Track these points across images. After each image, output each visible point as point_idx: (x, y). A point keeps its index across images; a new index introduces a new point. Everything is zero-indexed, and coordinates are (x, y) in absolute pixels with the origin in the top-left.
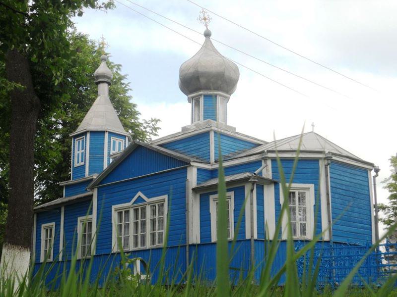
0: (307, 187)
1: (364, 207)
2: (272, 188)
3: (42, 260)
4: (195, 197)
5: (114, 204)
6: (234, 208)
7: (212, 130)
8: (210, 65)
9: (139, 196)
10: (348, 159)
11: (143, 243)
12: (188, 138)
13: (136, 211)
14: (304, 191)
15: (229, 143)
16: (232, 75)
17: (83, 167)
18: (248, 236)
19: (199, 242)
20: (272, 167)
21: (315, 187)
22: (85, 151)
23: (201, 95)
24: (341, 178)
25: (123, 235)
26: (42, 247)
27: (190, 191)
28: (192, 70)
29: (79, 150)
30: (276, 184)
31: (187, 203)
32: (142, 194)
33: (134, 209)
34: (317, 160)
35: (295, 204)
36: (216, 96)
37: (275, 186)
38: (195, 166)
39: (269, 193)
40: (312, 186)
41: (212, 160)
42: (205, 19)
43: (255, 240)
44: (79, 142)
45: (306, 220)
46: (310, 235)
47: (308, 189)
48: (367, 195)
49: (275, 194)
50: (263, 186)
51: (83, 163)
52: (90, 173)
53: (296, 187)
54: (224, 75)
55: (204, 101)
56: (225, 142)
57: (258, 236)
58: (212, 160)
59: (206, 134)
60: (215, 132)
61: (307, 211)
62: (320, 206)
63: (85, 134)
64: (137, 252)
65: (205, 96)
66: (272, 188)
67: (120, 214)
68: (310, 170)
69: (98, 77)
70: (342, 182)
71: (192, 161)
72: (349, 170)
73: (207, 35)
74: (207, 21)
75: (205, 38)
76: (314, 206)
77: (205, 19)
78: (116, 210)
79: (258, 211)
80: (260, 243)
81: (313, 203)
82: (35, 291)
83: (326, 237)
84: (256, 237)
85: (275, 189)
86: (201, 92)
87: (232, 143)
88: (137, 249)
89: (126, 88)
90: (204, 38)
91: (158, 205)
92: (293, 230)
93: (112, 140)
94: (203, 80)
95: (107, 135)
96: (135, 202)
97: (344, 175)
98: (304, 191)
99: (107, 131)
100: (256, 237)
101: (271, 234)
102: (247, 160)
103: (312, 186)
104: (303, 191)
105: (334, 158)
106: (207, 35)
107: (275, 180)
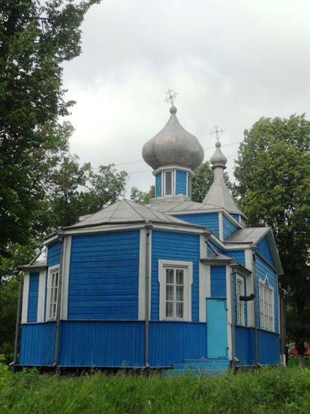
6: (192, 283)
11: (180, 312)
14: (172, 268)
18: (141, 317)
24: (91, 249)
25: (175, 298)
26: (40, 288)
32: (162, 260)
34: (138, 231)
38: (69, 235)
47: (186, 267)
60: (224, 215)
64: (181, 325)
67: (169, 273)
72: (128, 237)
73: (173, 111)
80: (32, 327)
81: (191, 282)
82: (192, 359)
84: (149, 319)
88: (169, 319)
91: (177, 271)
100: (149, 319)
105: (155, 226)
106: (173, 111)
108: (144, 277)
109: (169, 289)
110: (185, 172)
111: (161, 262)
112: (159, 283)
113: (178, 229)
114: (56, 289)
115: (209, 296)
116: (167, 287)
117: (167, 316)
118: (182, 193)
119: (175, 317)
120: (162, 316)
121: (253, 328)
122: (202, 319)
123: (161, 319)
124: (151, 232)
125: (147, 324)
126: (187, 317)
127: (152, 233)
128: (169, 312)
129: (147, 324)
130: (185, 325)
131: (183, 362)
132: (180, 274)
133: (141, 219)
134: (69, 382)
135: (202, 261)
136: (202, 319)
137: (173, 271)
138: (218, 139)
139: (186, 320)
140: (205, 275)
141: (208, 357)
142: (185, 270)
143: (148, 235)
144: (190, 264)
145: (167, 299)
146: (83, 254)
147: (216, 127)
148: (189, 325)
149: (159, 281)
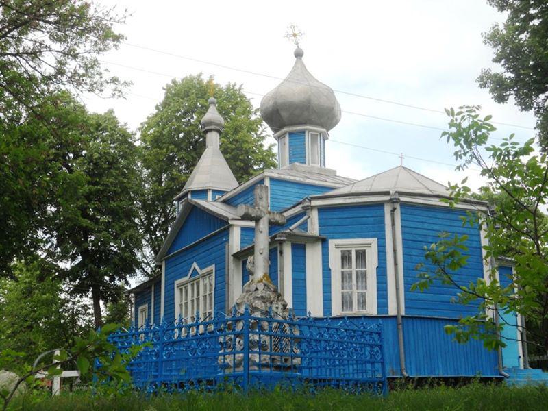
0: (367, 242)
1: (469, 265)
2: (319, 247)
4: (237, 266)
5: (176, 280)
7: (266, 176)
8: (296, 93)
10: (437, 199)
11: (363, 302)
12: (249, 188)
14: (365, 248)
15: (296, 191)
16: (324, 102)
20: (319, 219)
21: (378, 242)
24: (426, 226)
27: (231, 258)
28: (271, 103)
30: (324, 241)
31: (227, 273)
34: (380, 205)
35: (351, 268)
36: (303, 132)
37: (322, 244)
38: (238, 226)
39: (313, 256)
40: (374, 241)
42: (295, 35)
43: (403, 317)
45: (366, 289)
47: (369, 245)
48: (476, 248)
49: (323, 255)
50: (305, 245)
53: (341, 243)
55: (290, 140)
56: (290, 190)
57: (405, 311)
61: (368, 276)
62: (385, 268)
65: (291, 134)
66: (319, 247)
67: (345, 258)
68: (372, 219)
69: (205, 125)
70: (426, 232)
71: (230, 218)
73: (299, 55)
74: (298, 37)
75: (295, 59)
76: (377, 268)
77: (295, 35)
78: (178, 287)
79: (294, 280)
83: (392, 311)
85: (323, 247)
86: (285, 129)
87: (300, 191)
88: (348, 313)
89: (262, 135)
92: (346, 302)
94: (284, 114)
96: (191, 277)
97: (431, 221)
98: (365, 248)
99: (210, 190)
101: (315, 309)
102: (294, 212)
103: (374, 241)
104: (362, 249)
105: (403, 199)
106: (299, 55)
107: (324, 236)
108: (392, 250)
110: (303, 132)
112: (330, 269)
114: (210, 294)
117: (343, 311)
119: (355, 311)
124: (398, 206)
126: (372, 309)
127: (401, 208)
132: (361, 256)
134: (325, 373)
137: (350, 252)
142: (368, 250)
143: (394, 209)
145: (343, 289)
146: (415, 231)
147: (287, 36)
149: (330, 267)
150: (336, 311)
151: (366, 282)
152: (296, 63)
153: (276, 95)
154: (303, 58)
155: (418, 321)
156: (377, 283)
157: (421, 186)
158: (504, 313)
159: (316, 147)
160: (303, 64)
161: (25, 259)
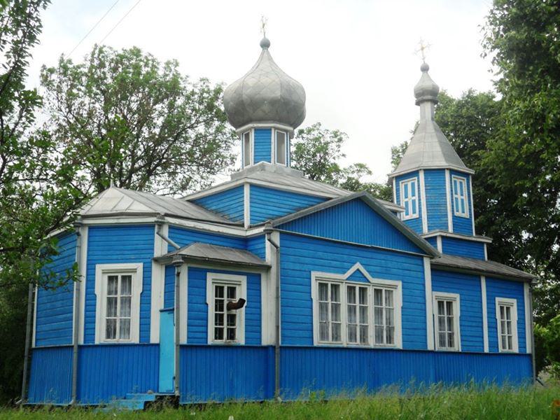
3: (34, 346)
9: (358, 270)
13: (351, 290)
17: (419, 220)
19: (138, 342)
22: (452, 197)
23: (250, 129)
29: (406, 197)
32: (102, 265)
33: (348, 287)
41: (247, 222)
44: (406, 187)
46: (134, 338)
47: (134, 271)
51: (416, 216)
52: (430, 228)
54: (242, 101)
55: (255, 136)
58: (247, 222)
59: (241, 187)
63: (415, 173)
64: (125, 347)
65: (257, 130)
67: (323, 286)
73: (265, 45)
75: (261, 49)
90: (421, 73)
92: (110, 332)
93: (453, 179)
95: (447, 174)
106: (265, 45)
109: (323, 307)
110: (268, 130)
111: (99, 268)
113: (122, 221)
115: (162, 308)
116: (321, 304)
118: (264, 159)
119: (385, 345)
120: (100, 337)
121: (273, 347)
122: (154, 339)
123: (97, 342)
125: (75, 350)
126: (134, 338)
128: (323, 335)
129: (277, 351)
130: (391, 353)
131: (125, 398)
132: (127, 280)
133: (150, 211)
135: (157, 260)
136: (154, 339)
138: (424, 59)
139: (132, 342)
140: (158, 275)
141: (160, 391)
144: (139, 266)
147: (421, 42)
148: (239, 350)
149: (96, 293)
150: (100, 337)
151: (130, 307)
152: (262, 54)
153: (243, 86)
154: (269, 49)
155: (322, 351)
156: (188, 311)
157: (296, 203)
158: (26, 398)
159: (283, 146)
160: (270, 59)
161: (548, 223)
